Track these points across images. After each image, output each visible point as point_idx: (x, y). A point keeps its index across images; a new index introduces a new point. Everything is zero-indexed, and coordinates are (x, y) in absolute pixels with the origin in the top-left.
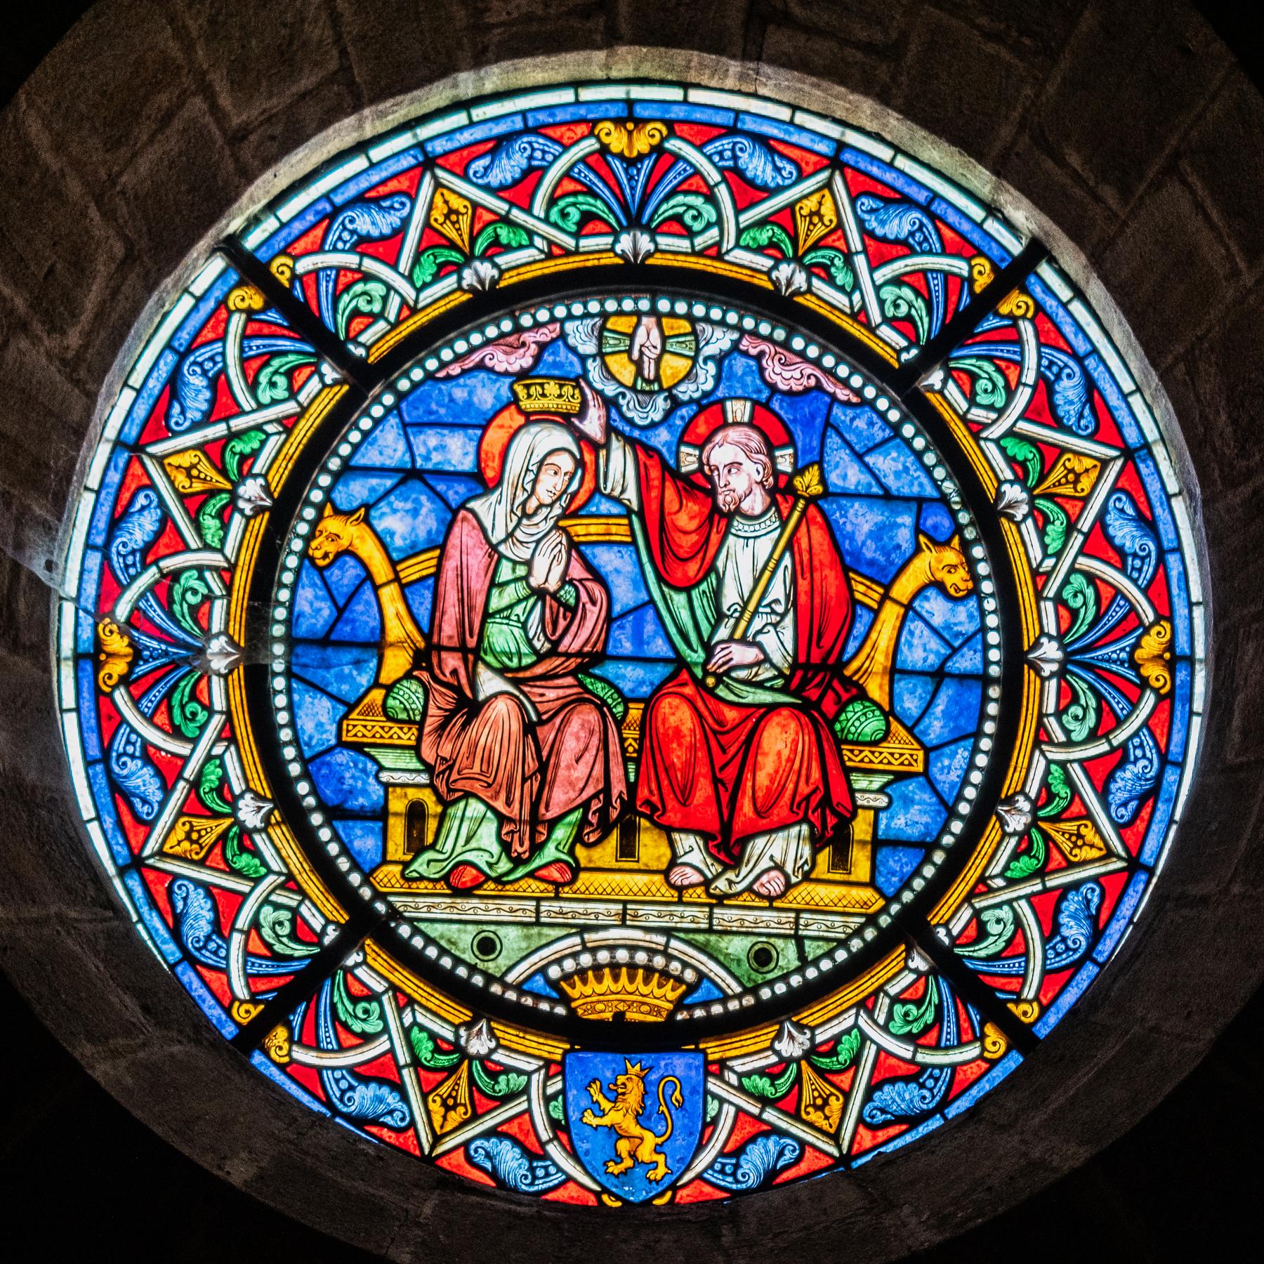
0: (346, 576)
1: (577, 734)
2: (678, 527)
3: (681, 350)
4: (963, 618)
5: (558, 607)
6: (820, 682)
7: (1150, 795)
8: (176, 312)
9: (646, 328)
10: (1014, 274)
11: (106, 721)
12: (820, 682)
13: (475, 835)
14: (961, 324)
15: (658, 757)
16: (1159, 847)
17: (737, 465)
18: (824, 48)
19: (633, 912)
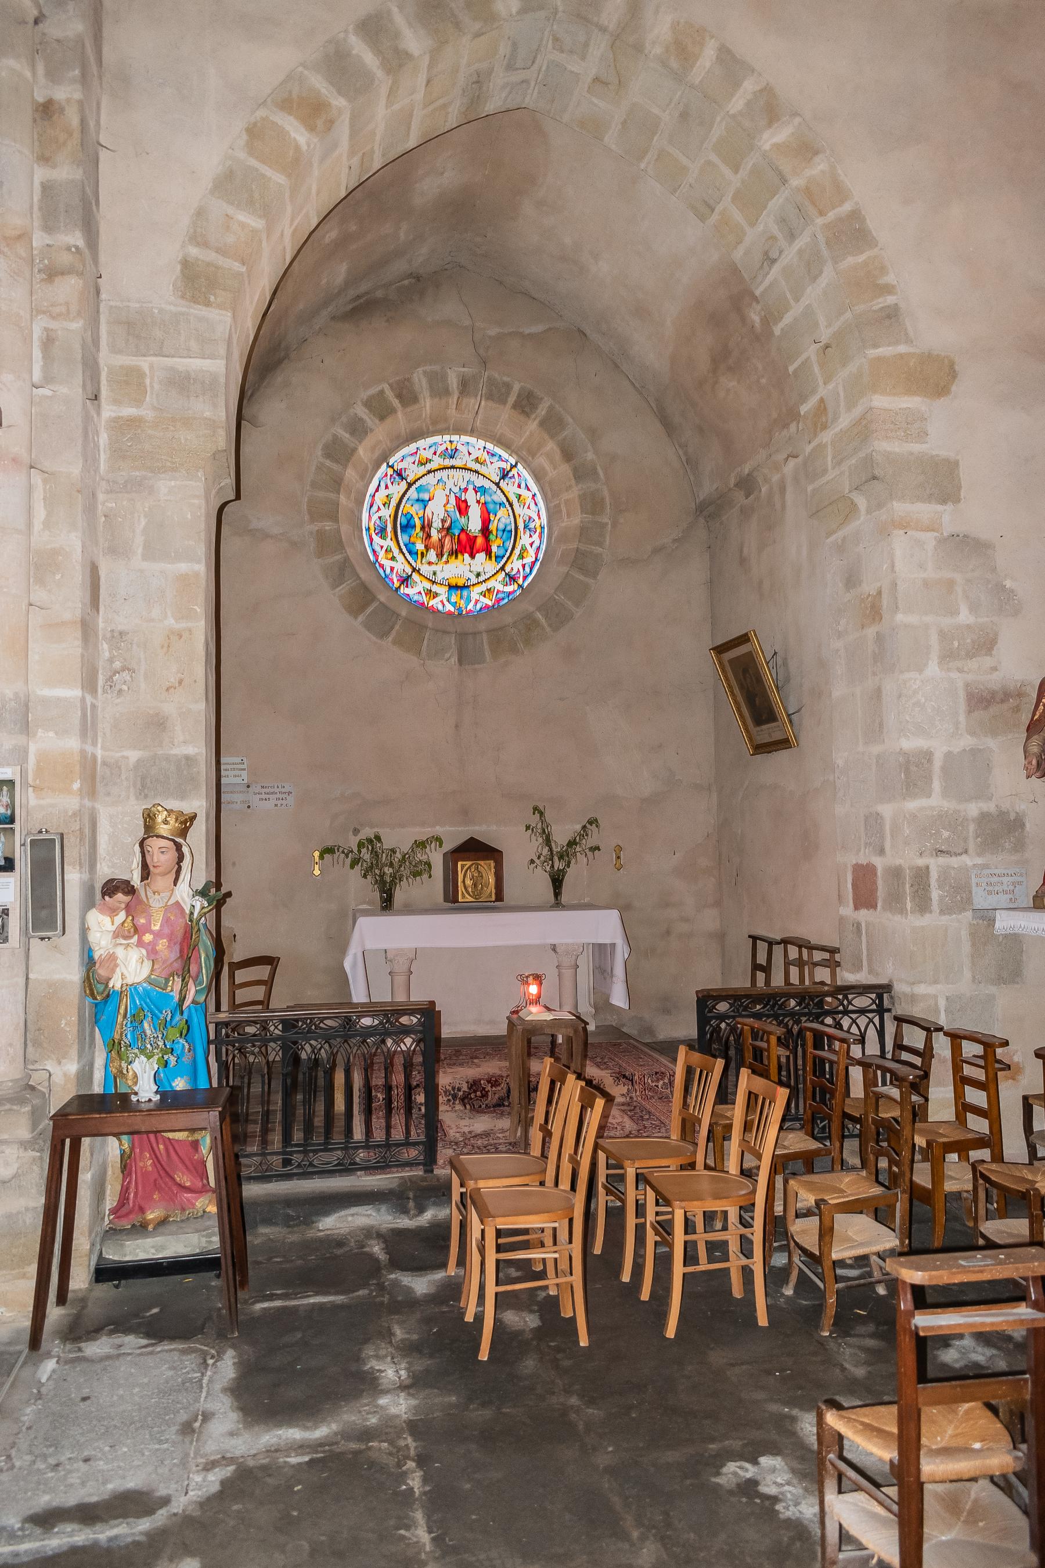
0: (409, 516)
1: (447, 540)
2: (463, 507)
3: (460, 478)
4: (508, 521)
5: (443, 521)
6: (485, 531)
7: (538, 549)
8: (505, 455)
9: (457, 474)
10: (512, 467)
11: (371, 540)
12: (485, 531)
13: (432, 555)
14: (504, 475)
15: (266, 1089)
16: (541, 556)
17: (471, 497)
18: (913, 1456)
19: (459, 568)
